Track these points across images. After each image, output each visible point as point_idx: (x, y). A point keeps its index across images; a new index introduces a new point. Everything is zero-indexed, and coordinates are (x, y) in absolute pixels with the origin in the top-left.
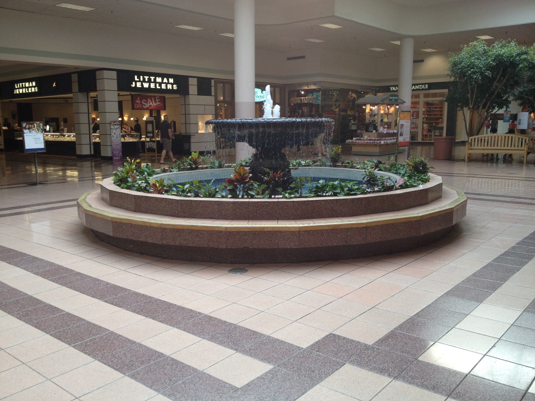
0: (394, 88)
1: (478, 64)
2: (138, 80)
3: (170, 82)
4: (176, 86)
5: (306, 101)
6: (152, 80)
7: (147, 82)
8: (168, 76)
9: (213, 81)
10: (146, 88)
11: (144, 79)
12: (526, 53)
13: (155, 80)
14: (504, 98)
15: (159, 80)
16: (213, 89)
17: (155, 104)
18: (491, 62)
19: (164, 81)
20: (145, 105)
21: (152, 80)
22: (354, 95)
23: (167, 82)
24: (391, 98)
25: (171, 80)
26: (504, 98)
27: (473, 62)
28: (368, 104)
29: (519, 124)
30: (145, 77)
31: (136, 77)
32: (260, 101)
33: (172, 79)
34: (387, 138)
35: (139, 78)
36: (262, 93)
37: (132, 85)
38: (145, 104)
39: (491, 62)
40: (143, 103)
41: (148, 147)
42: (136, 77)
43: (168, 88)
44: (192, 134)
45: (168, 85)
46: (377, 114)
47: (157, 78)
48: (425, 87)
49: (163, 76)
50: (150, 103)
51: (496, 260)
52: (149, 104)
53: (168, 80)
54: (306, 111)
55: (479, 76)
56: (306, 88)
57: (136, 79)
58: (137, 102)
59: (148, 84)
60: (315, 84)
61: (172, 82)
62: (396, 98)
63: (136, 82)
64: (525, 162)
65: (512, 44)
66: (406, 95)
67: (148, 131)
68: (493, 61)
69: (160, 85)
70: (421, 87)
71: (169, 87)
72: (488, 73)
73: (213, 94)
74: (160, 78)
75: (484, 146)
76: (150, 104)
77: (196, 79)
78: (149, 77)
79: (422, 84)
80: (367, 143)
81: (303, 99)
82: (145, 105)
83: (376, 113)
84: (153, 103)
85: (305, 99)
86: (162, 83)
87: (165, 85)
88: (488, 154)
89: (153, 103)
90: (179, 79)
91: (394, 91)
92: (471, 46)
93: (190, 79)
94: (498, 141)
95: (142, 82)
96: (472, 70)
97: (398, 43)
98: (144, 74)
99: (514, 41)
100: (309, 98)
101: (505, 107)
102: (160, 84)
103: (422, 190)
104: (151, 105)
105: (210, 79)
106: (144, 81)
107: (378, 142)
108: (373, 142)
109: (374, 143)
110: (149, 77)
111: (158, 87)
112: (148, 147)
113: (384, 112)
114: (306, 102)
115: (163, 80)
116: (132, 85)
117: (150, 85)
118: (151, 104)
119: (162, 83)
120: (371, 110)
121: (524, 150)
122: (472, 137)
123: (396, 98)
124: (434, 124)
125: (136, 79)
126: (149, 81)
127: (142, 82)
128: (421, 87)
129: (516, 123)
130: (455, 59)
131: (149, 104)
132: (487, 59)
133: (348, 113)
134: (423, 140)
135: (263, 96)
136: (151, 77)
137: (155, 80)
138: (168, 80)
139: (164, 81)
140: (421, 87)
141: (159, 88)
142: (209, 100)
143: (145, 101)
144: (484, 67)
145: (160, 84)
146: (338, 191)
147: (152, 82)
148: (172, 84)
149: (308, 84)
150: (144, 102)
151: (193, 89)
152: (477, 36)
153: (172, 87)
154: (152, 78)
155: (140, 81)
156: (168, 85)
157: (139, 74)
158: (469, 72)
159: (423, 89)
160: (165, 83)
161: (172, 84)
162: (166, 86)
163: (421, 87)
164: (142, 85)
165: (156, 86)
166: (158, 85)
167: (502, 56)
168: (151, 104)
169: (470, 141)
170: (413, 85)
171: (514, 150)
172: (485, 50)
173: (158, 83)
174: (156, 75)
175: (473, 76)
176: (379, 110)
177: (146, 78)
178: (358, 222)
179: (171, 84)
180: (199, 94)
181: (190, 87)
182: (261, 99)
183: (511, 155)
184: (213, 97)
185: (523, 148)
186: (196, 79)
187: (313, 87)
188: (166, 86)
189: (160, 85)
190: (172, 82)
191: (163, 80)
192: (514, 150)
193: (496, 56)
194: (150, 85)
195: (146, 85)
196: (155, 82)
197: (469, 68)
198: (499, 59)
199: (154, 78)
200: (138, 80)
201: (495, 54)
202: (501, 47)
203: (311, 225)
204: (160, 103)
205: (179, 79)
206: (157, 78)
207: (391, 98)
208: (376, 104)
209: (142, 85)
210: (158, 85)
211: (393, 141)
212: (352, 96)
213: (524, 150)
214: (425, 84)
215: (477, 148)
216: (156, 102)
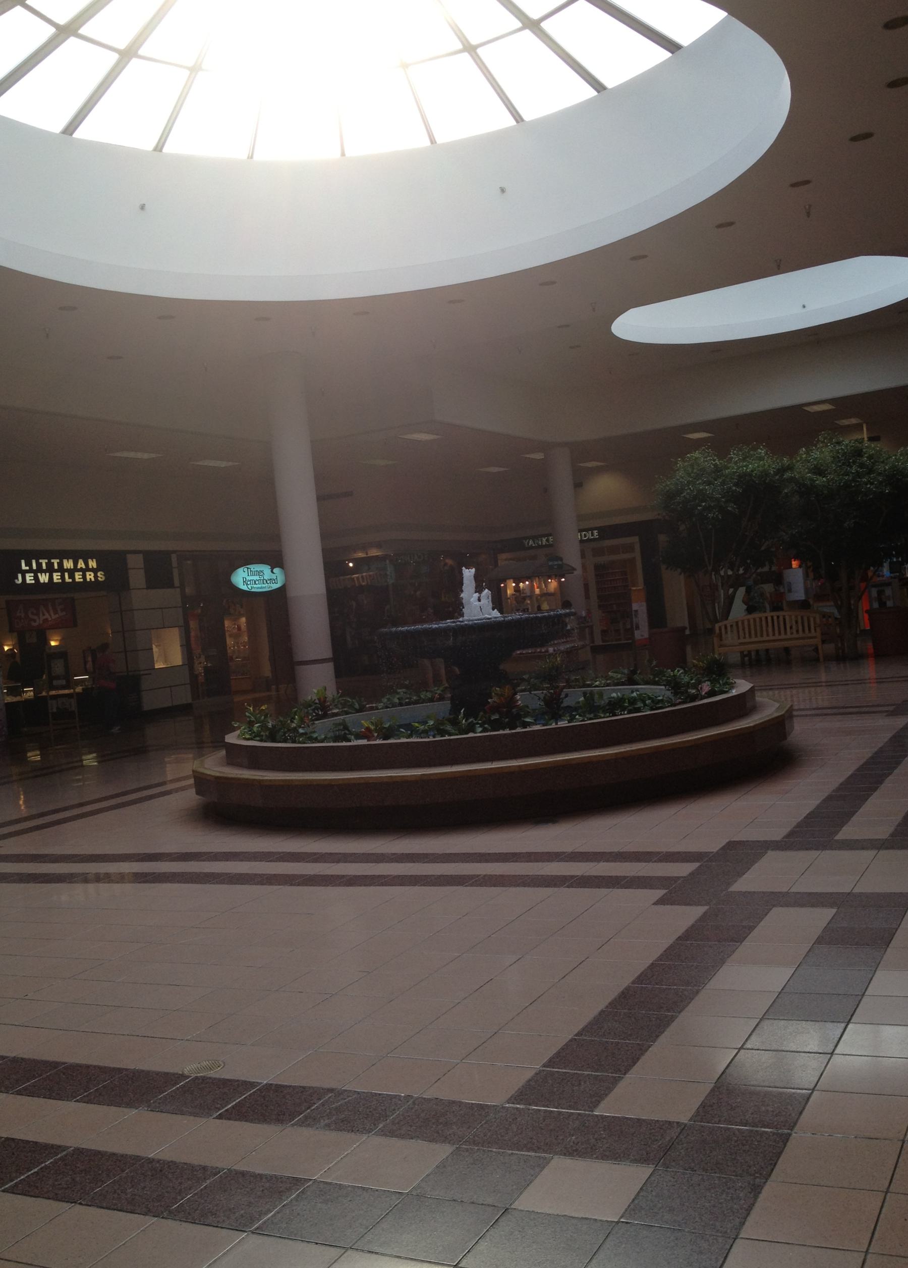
0: (531, 542)
1: (712, 494)
2: (27, 568)
3: (90, 567)
4: (103, 573)
5: (363, 582)
6: (56, 567)
7: (45, 572)
8: (86, 555)
9: (174, 558)
10: (44, 583)
11: (39, 565)
12: (790, 468)
13: (61, 564)
14: (763, 548)
15: (68, 564)
16: (176, 573)
17: (54, 617)
18: (734, 488)
19: (79, 567)
20: (35, 621)
21: (56, 567)
22: (449, 562)
23: (84, 567)
24: (550, 563)
25: (93, 564)
26: (763, 548)
27: (702, 490)
28: (510, 578)
29: (790, 591)
30: (40, 561)
31: (23, 563)
32: (270, 589)
33: (94, 560)
34: (556, 642)
35: (29, 564)
36: (272, 572)
37: (16, 581)
38: (35, 617)
39: (734, 488)
40: (31, 616)
41: (55, 710)
42: (23, 563)
43: (88, 580)
44: (142, 673)
45: (88, 573)
46: (530, 597)
47: (65, 562)
48: (592, 535)
49: (75, 556)
50: (44, 615)
51: (824, 800)
52: (42, 618)
53: (86, 564)
54: (365, 602)
55: (717, 513)
56: (361, 555)
57: (24, 567)
58: (18, 614)
59: (48, 574)
60: (379, 546)
61: (95, 566)
62: (560, 563)
63: (24, 573)
64: (821, 659)
65: (761, 453)
66: (571, 554)
67: (53, 675)
68: (736, 485)
69: (72, 576)
70: (585, 537)
71: (90, 576)
72: (731, 507)
73: (177, 582)
74: (71, 562)
75: (768, 635)
76: (45, 617)
77: (141, 556)
78: (49, 561)
79: (587, 530)
80: (521, 654)
81: (358, 578)
82: (35, 621)
83: (528, 594)
84: (50, 616)
85: (362, 577)
86: (75, 569)
87: (81, 573)
88: (750, 652)
89: (50, 616)
90: (108, 560)
91: (531, 548)
92: (690, 460)
93: (129, 557)
94: (749, 629)
95: (35, 573)
96: (704, 504)
97: (539, 456)
98: (39, 555)
99: (764, 446)
100: (370, 576)
101: (767, 563)
102: (72, 573)
103: (735, 696)
104: (47, 619)
105: (168, 554)
106: (40, 569)
107: (543, 651)
108: (533, 651)
109: (534, 653)
110: (49, 561)
111: (67, 580)
112: (55, 710)
113: (540, 591)
114: (364, 584)
115: (76, 564)
116: (16, 581)
117: (51, 578)
118: (47, 616)
119: (75, 569)
120: (517, 589)
121: (815, 637)
122: (720, 624)
123: (560, 563)
124: (614, 606)
125: (24, 567)
126: (50, 570)
127: (35, 573)
128: (585, 537)
129: (782, 591)
130: (667, 485)
131: (42, 618)
132: (723, 483)
133: (443, 599)
134: (603, 641)
135: (275, 578)
136: (52, 561)
137: (61, 564)
138: (86, 564)
139: (79, 567)
140: (585, 536)
141: (71, 580)
142: (169, 596)
143: (35, 612)
144: (722, 497)
145: (72, 573)
146: (640, 704)
147: (56, 571)
148: (95, 570)
149: (364, 548)
150: (33, 613)
151: (137, 577)
152: (684, 434)
153: (96, 577)
154: (55, 562)
155: (31, 571)
156: (88, 573)
157: (29, 556)
158: (699, 508)
159: (589, 540)
160: (81, 570)
161: (95, 570)
162: (84, 577)
163: (585, 536)
164: (36, 578)
165: (63, 577)
166: (66, 575)
167: (750, 475)
168: (47, 616)
169: (717, 631)
170: (580, 531)
171: (797, 639)
172: (715, 465)
173: (68, 570)
174: (63, 555)
175: (707, 515)
176: (532, 587)
177: (44, 563)
178: (666, 743)
179: (92, 570)
180: (148, 588)
181: (131, 573)
182: (272, 585)
183: (787, 650)
184: (178, 590)
185: (813, 633)
186: (141, 556)
187: (374, 552)
188: (84, 577)
189: (72, 576)
190: (95, 566)
191: (76, 564)
192: (797, 639)
193: (740, 476)
194: (51, 578)
195: (44, 578)
196: (61, 569)
197: (697, 501)
198: (744, 479)
199: (58, 561)
200: (27, 568)
201: (736, 472)
202: (744, 459)
203: (628, 749)
204: (64, 613)
205: (108, 560)
206: (65, 562)
207: (550, 563)
208: (527, 578)
209: (36, 578)
210: (66, 575)
211: (568, 646)
212: (446, 564)
213: (815, 637)
214: (592, 529)
215: (780, 638)
216: (56, 612)
